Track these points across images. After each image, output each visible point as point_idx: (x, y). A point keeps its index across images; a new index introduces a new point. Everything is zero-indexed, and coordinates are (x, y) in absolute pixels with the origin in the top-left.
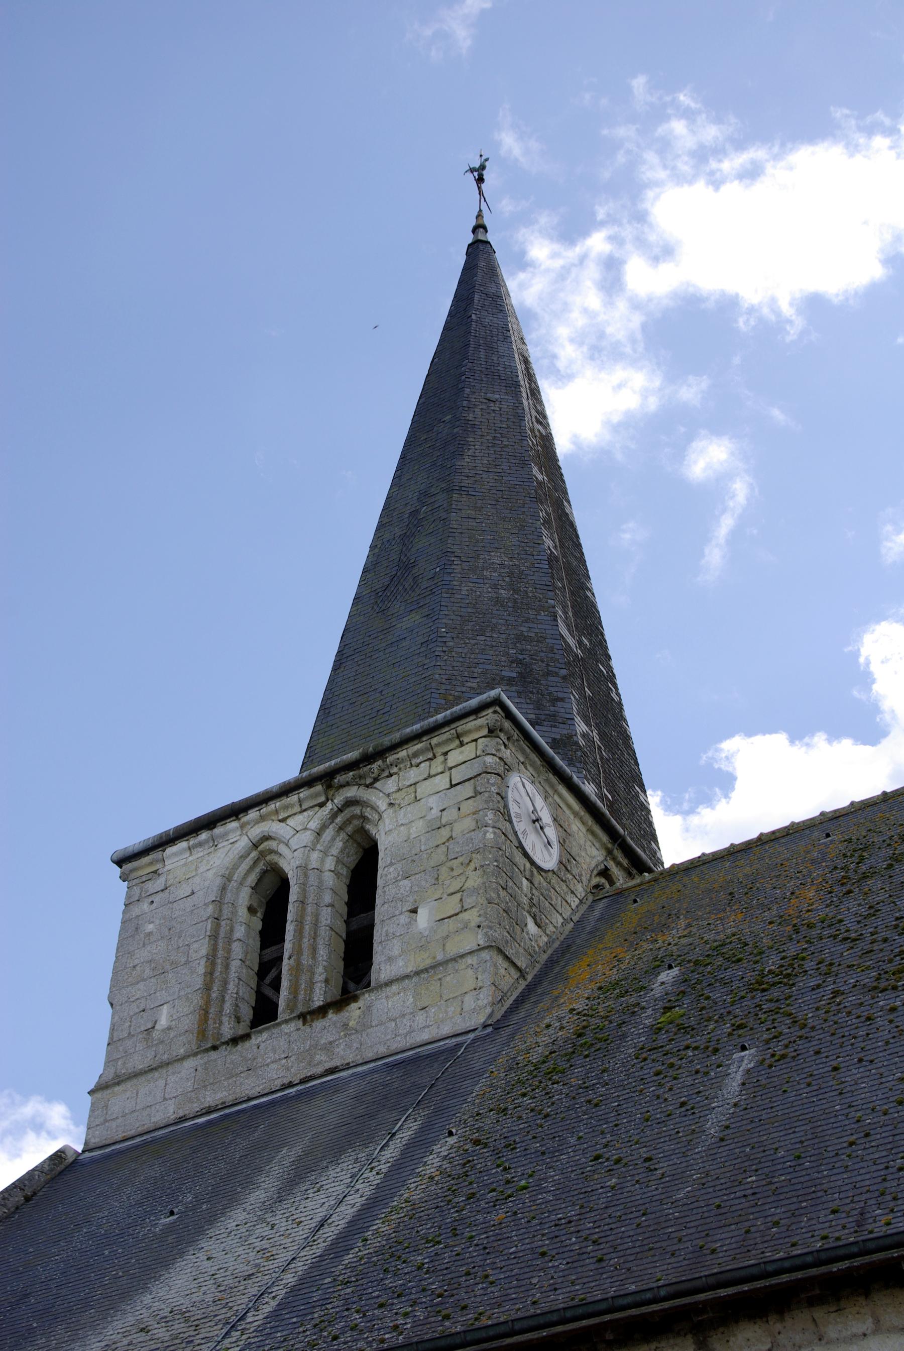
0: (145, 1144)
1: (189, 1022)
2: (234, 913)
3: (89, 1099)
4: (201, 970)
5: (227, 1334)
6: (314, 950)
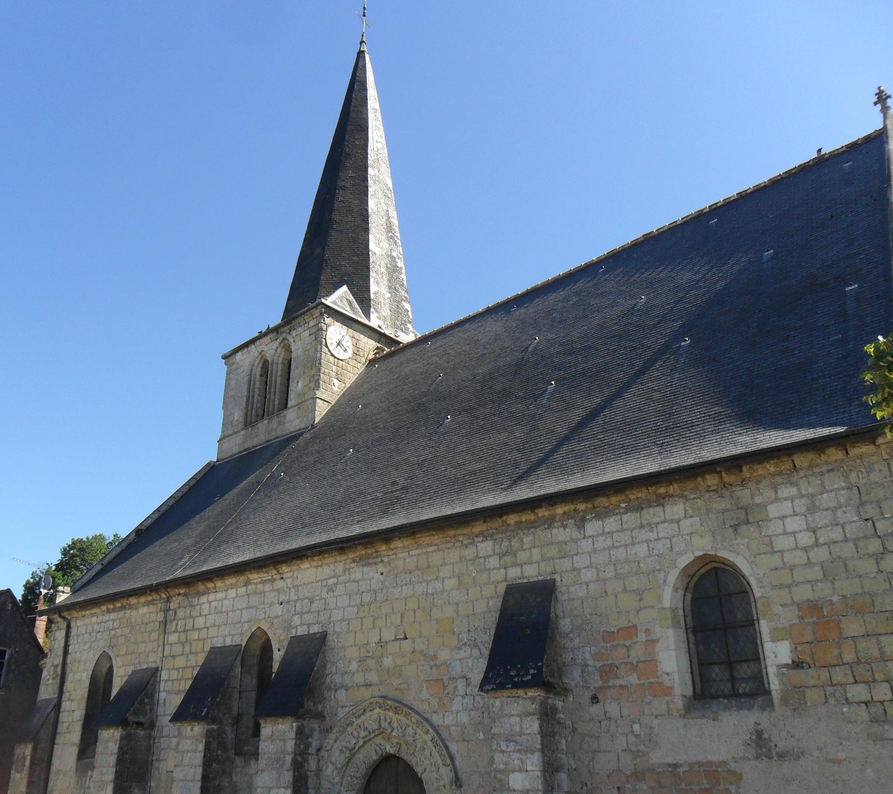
0: (230, 461)
1: (241, 419)
2: (255, 378)
3: (218, 443)
4: (245, 400)
5: (410, 581)
6: (275, 393)
